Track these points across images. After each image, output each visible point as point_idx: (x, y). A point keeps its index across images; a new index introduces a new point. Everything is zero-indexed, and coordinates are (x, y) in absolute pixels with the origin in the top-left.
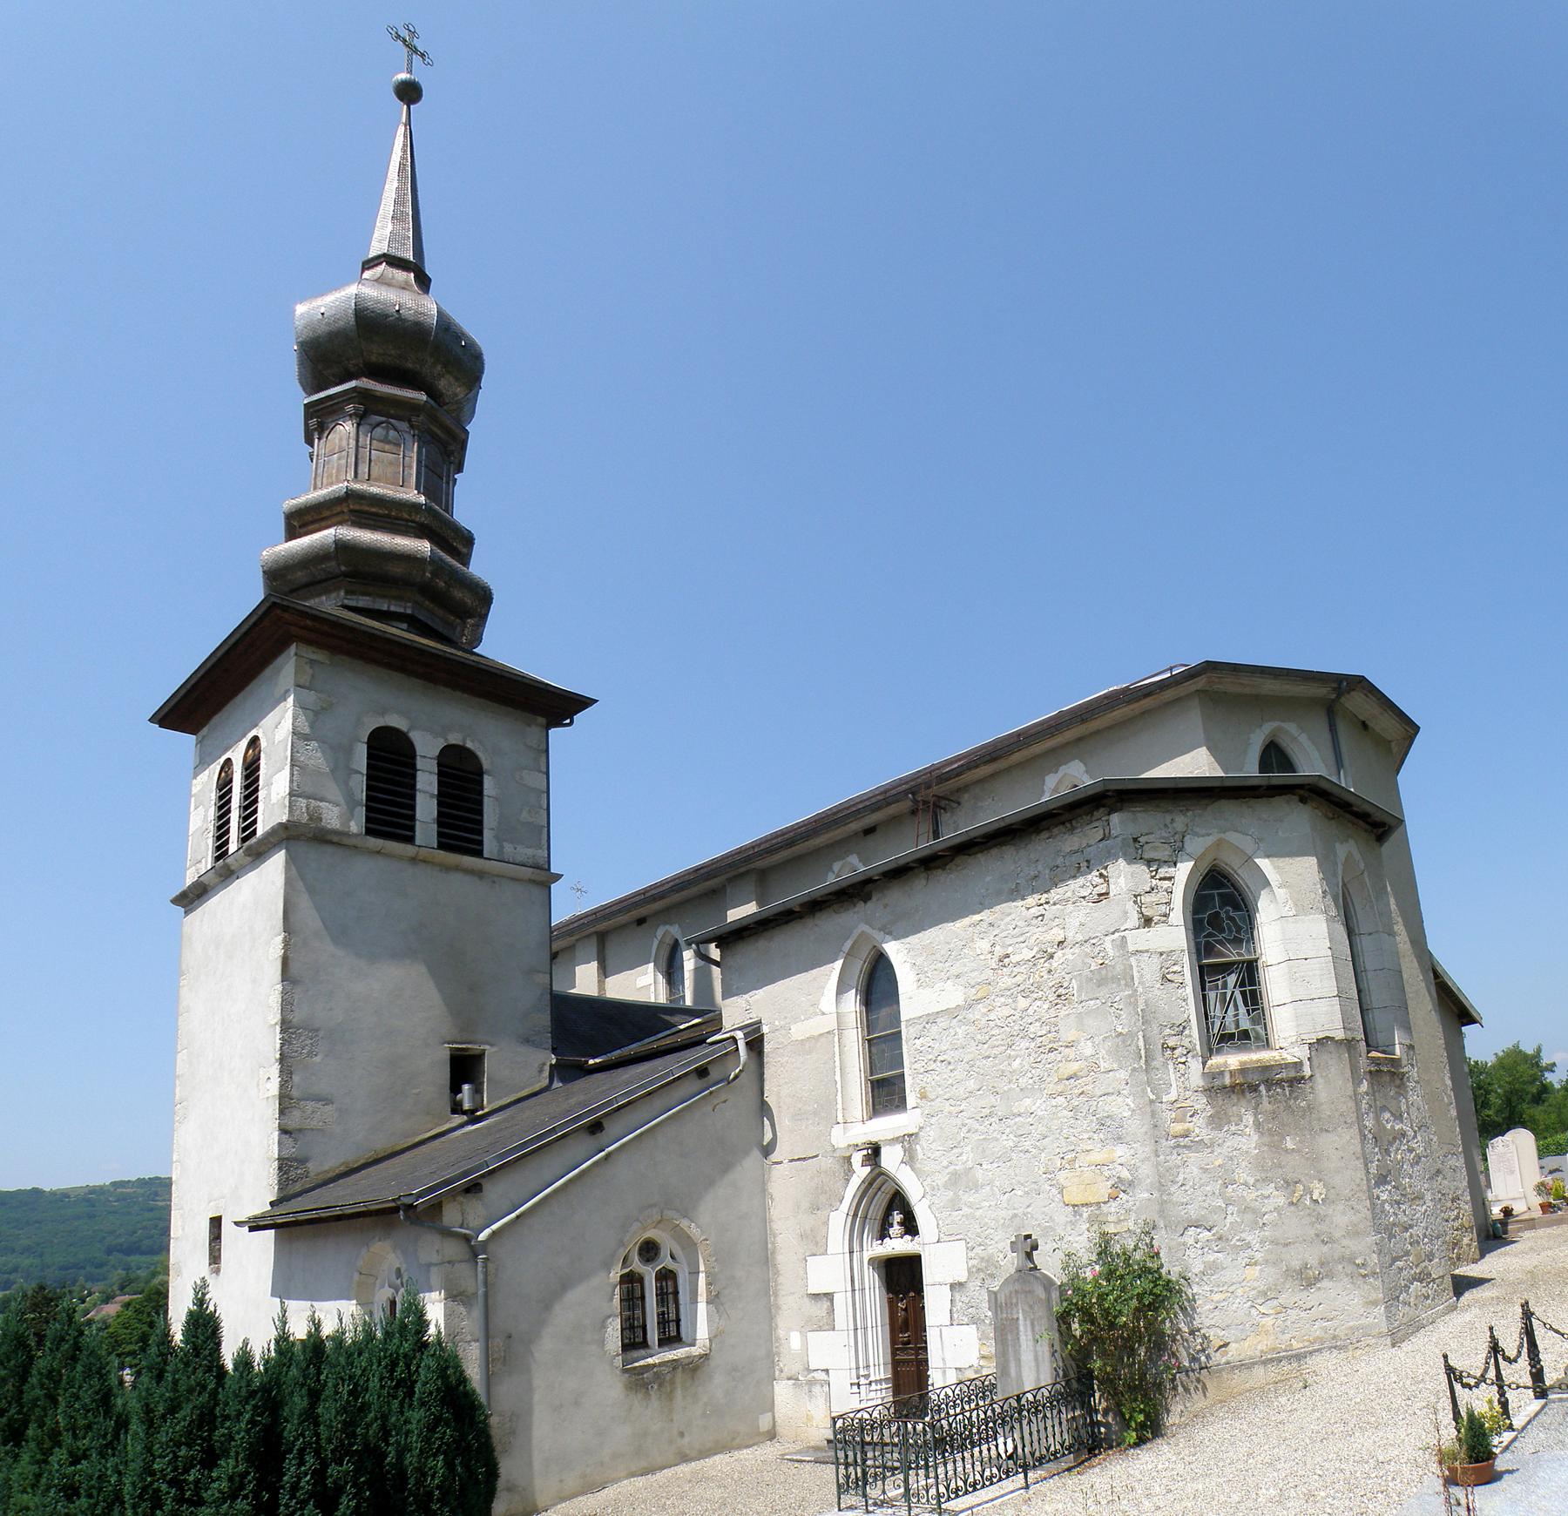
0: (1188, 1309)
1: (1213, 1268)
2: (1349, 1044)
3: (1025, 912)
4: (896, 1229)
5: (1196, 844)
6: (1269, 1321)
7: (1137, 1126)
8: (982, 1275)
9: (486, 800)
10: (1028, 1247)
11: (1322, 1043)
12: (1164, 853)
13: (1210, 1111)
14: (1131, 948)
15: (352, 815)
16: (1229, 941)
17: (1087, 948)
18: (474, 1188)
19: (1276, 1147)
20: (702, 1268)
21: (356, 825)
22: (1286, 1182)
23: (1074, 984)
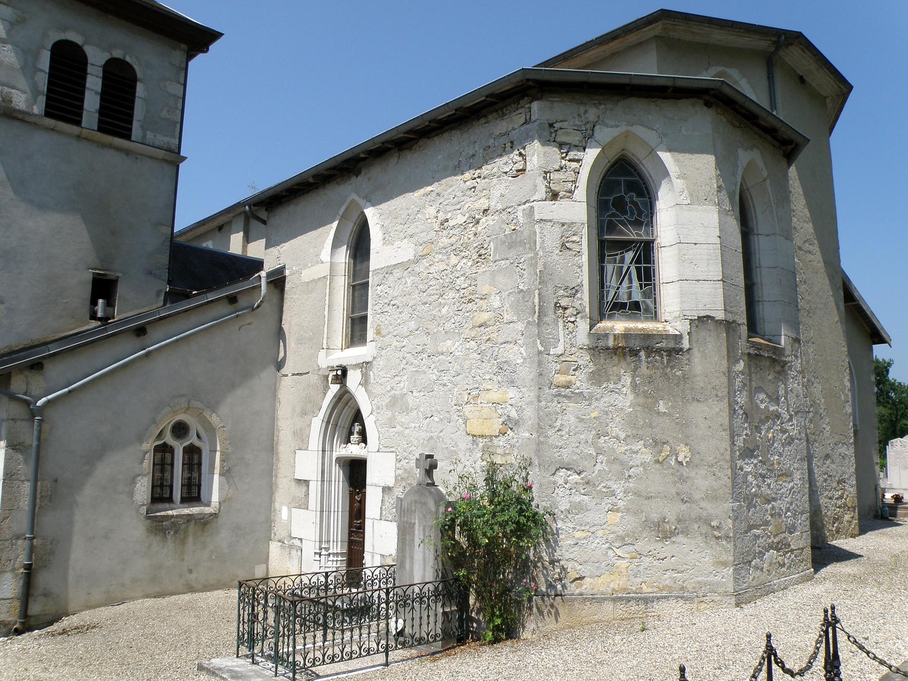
0: (551, 539)
1: (577, 508)
2: (729, 326)
3: (462, 184)
4: (355, 437)
5: (604, 134)
6: (623, 564)
7: (526, 373)
8: (404, 484)
9: (137, 101)
10: (430, 466)
11: (702, 321)
12: (575, 138)
13: (592, 368)
14: (537, 217)
15: (36, 102)
16: (631, 223)
17: (504, 216)
18: (37, 366)
19: (650, 408)
20: (218, 448)
21: (38, 109)
22: (655, 442)
23: (492, 245)
